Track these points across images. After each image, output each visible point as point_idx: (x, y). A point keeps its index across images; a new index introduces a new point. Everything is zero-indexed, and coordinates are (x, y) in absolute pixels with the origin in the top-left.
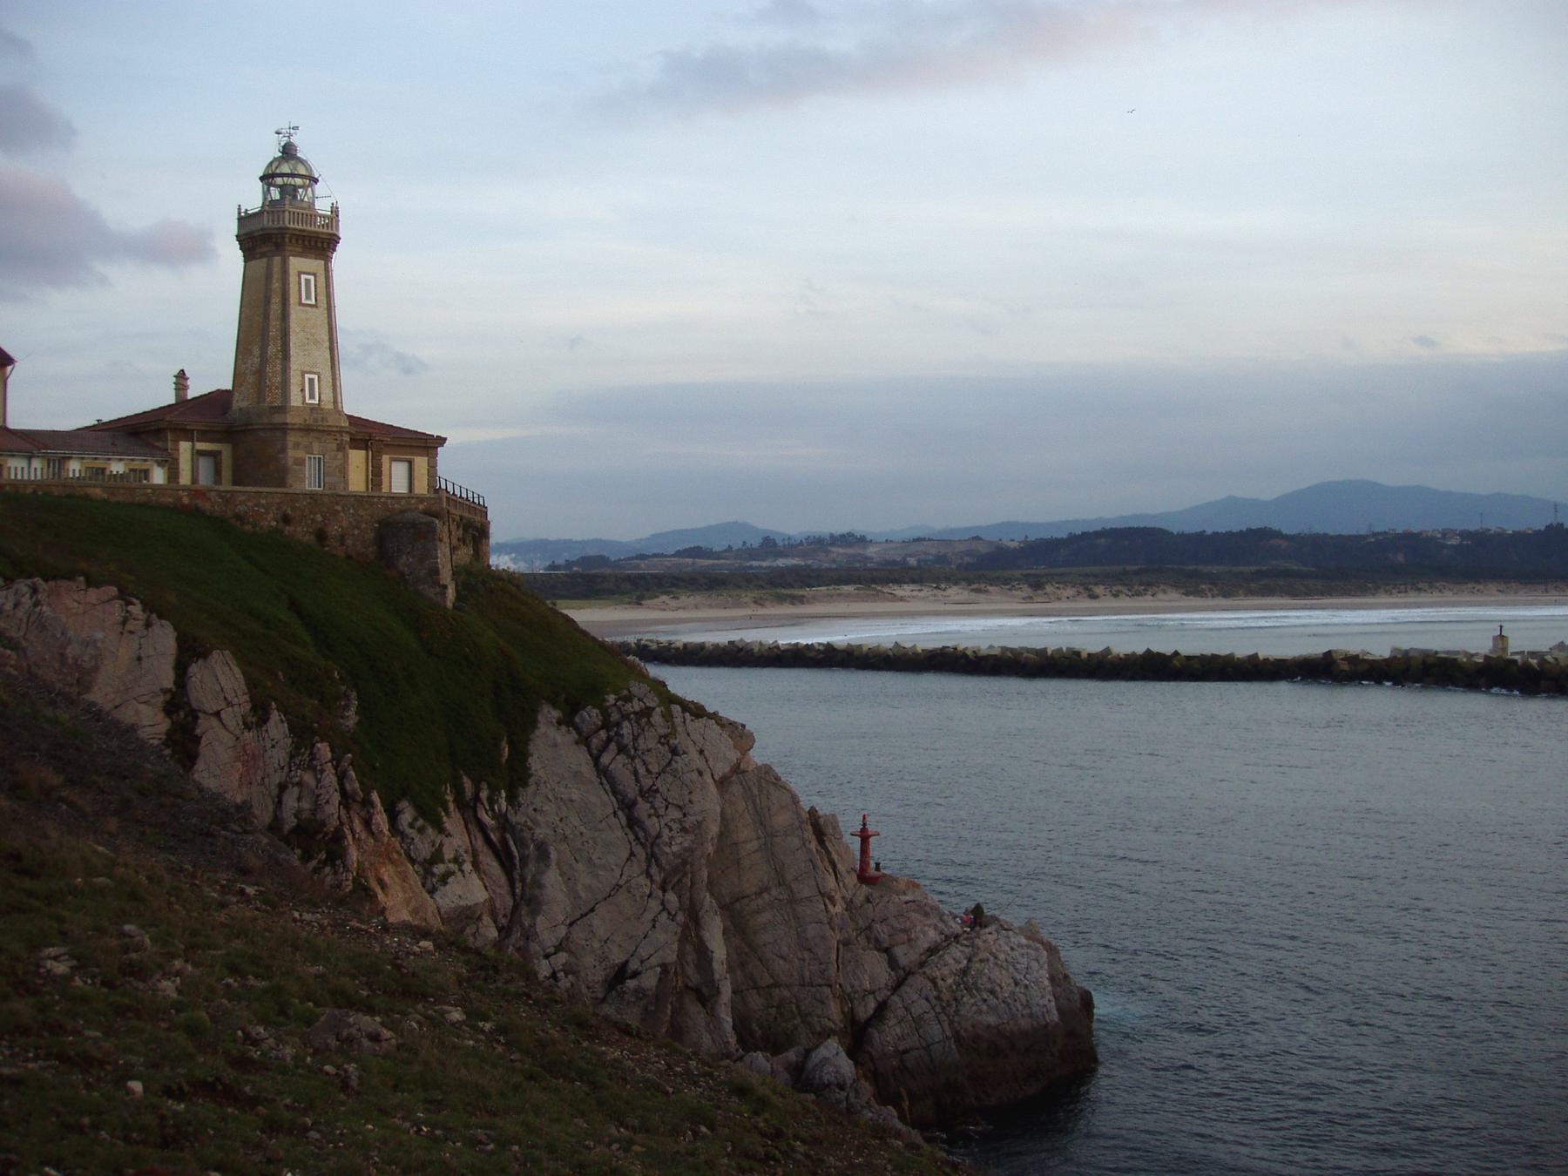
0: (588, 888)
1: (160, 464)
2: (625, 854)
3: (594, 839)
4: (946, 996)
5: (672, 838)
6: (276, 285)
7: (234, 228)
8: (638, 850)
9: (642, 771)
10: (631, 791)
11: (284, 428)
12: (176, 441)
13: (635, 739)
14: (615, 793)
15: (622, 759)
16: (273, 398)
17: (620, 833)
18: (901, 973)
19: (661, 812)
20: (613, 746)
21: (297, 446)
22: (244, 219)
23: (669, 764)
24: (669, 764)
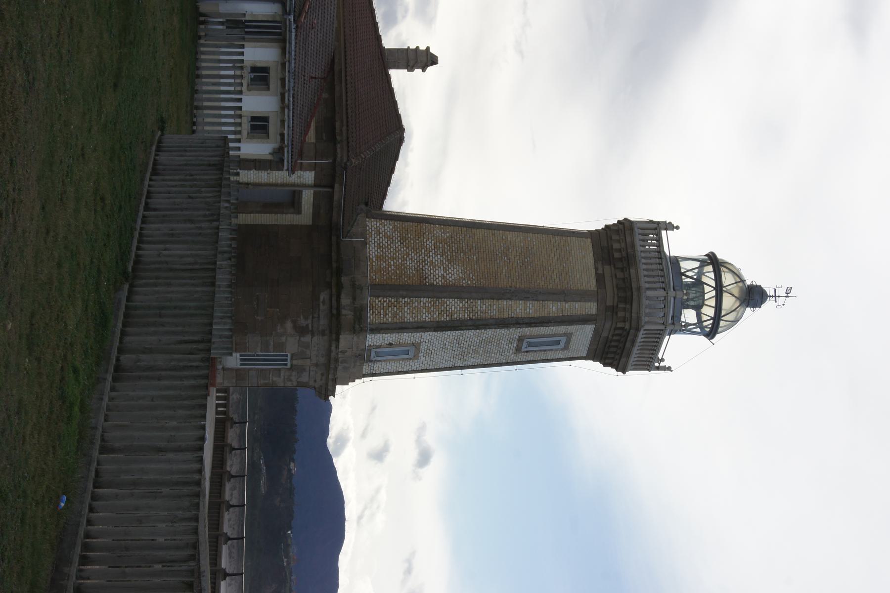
1: (279, 151)
6: (553, 308)
7: (638, 214)
11: (334, 331)
12: (313, 167)
16: (377, 309)
22: (657, 228)
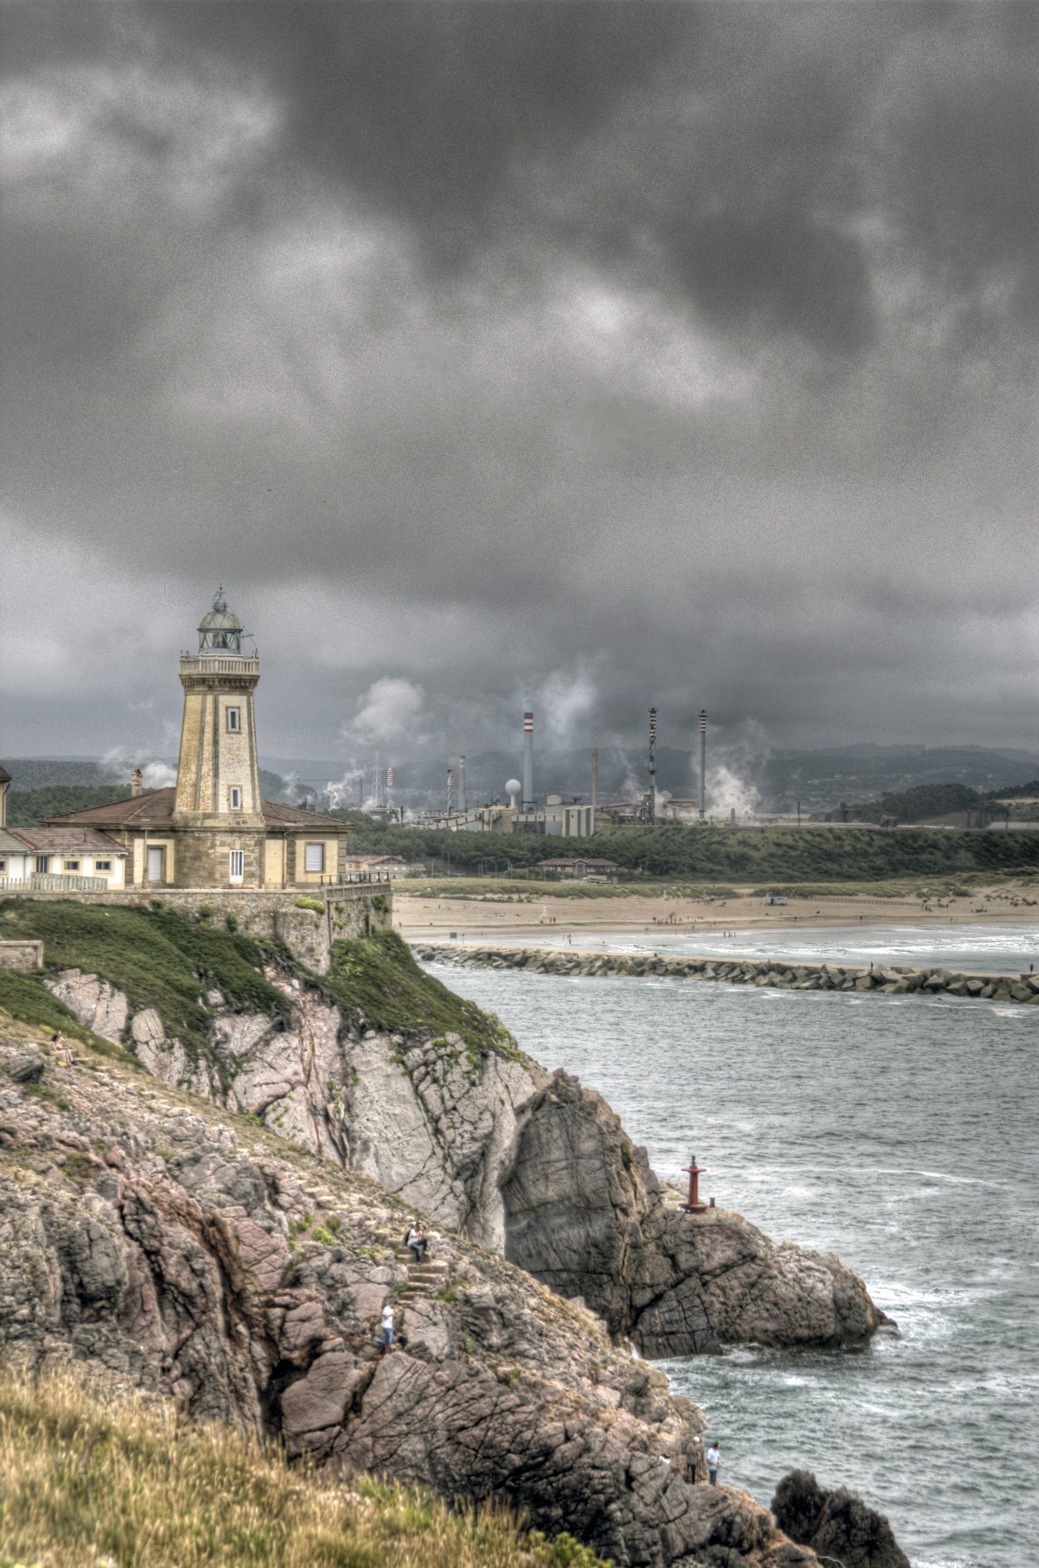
0: (400, 1175)
2: (428, 1153)
3: (408, 1142)
4: (733, 1301)
5: (462, 1144)
6: (209, 718)
8: (438, 1150)
9: (447, 1096)
10: (436, 1108)
12: (131, 840)
13: (445, 1073)
14: (427, 1111)
15: (434, 1087)
17: (426, 1139)
18: (682, 1275)
19: (458, 1125)
20: (429, 1078)
21: (223, 844)
23: (468, 1092)
24: (468, 1092)
